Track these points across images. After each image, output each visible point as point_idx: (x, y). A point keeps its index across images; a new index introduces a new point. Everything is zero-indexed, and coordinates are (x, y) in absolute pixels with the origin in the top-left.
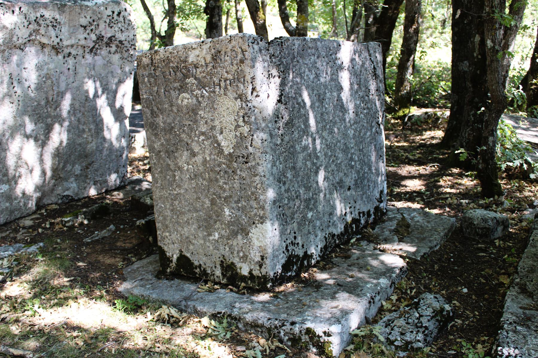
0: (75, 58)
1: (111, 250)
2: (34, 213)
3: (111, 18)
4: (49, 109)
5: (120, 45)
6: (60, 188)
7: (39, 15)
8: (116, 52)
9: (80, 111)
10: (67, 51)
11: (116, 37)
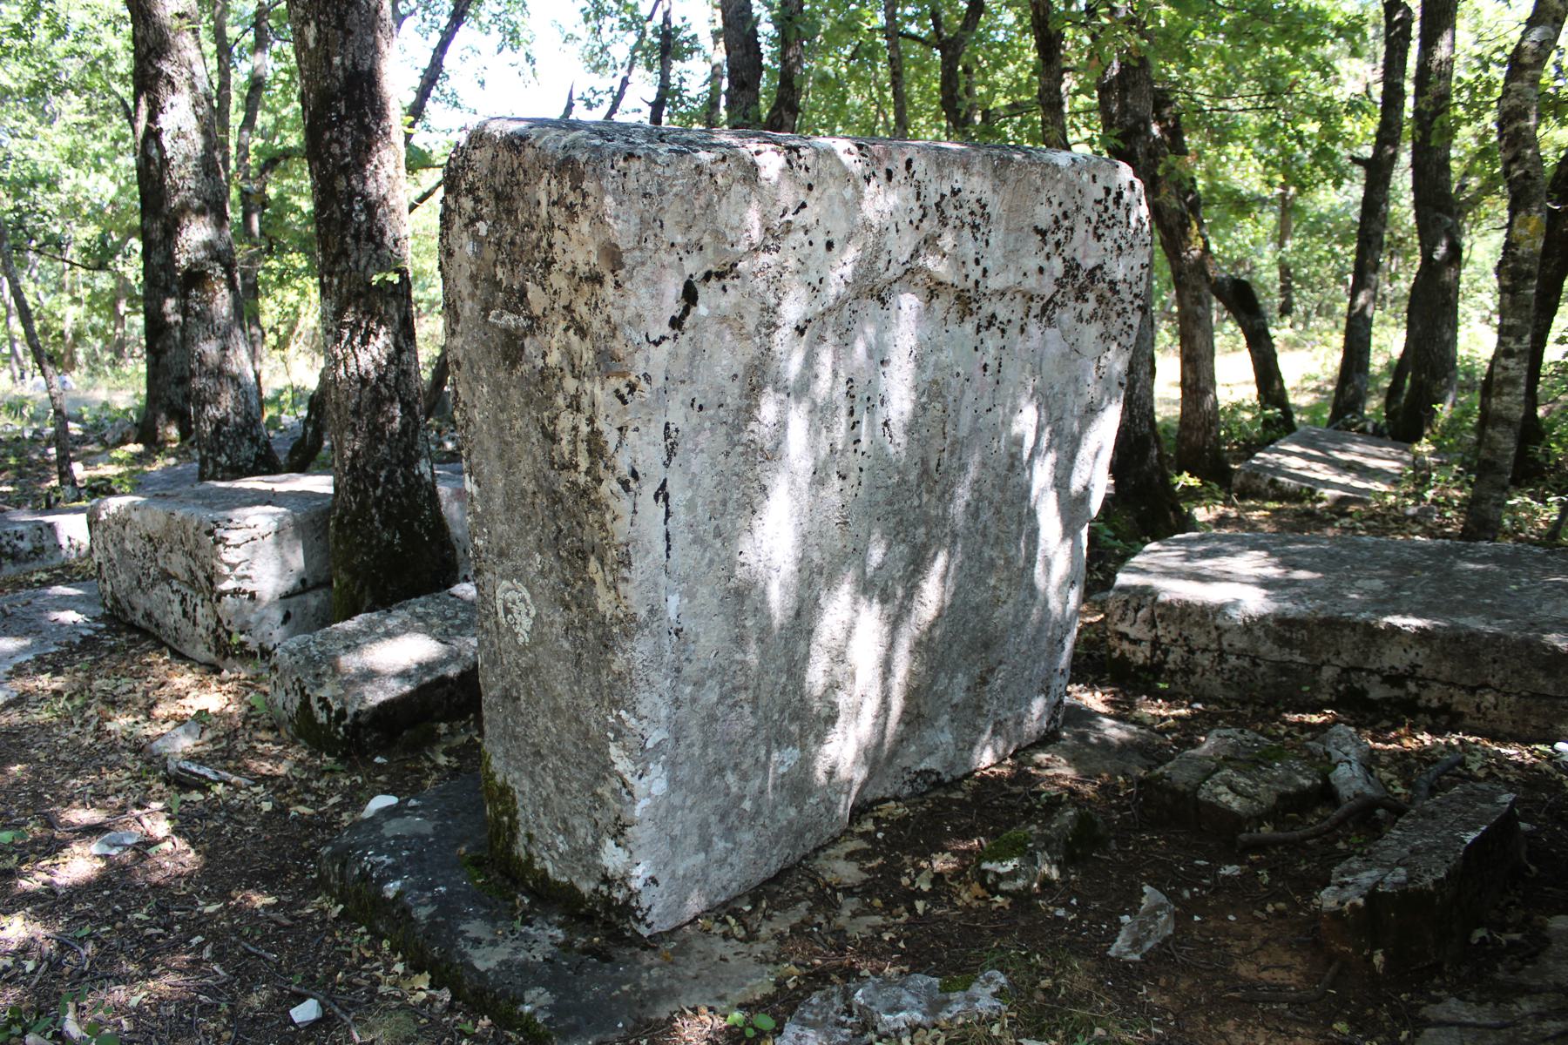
0: (1003, 331)
1: (1253, 1002)
2: (847, 833)
3: (1101, 208)
4: (925, 498)
5: (1109, 294)
6: (913, 748)
7: (947, 191)
8: (1094, 316)
9: (991, 503)
10: (988, 308)
11: (1106, 268)
